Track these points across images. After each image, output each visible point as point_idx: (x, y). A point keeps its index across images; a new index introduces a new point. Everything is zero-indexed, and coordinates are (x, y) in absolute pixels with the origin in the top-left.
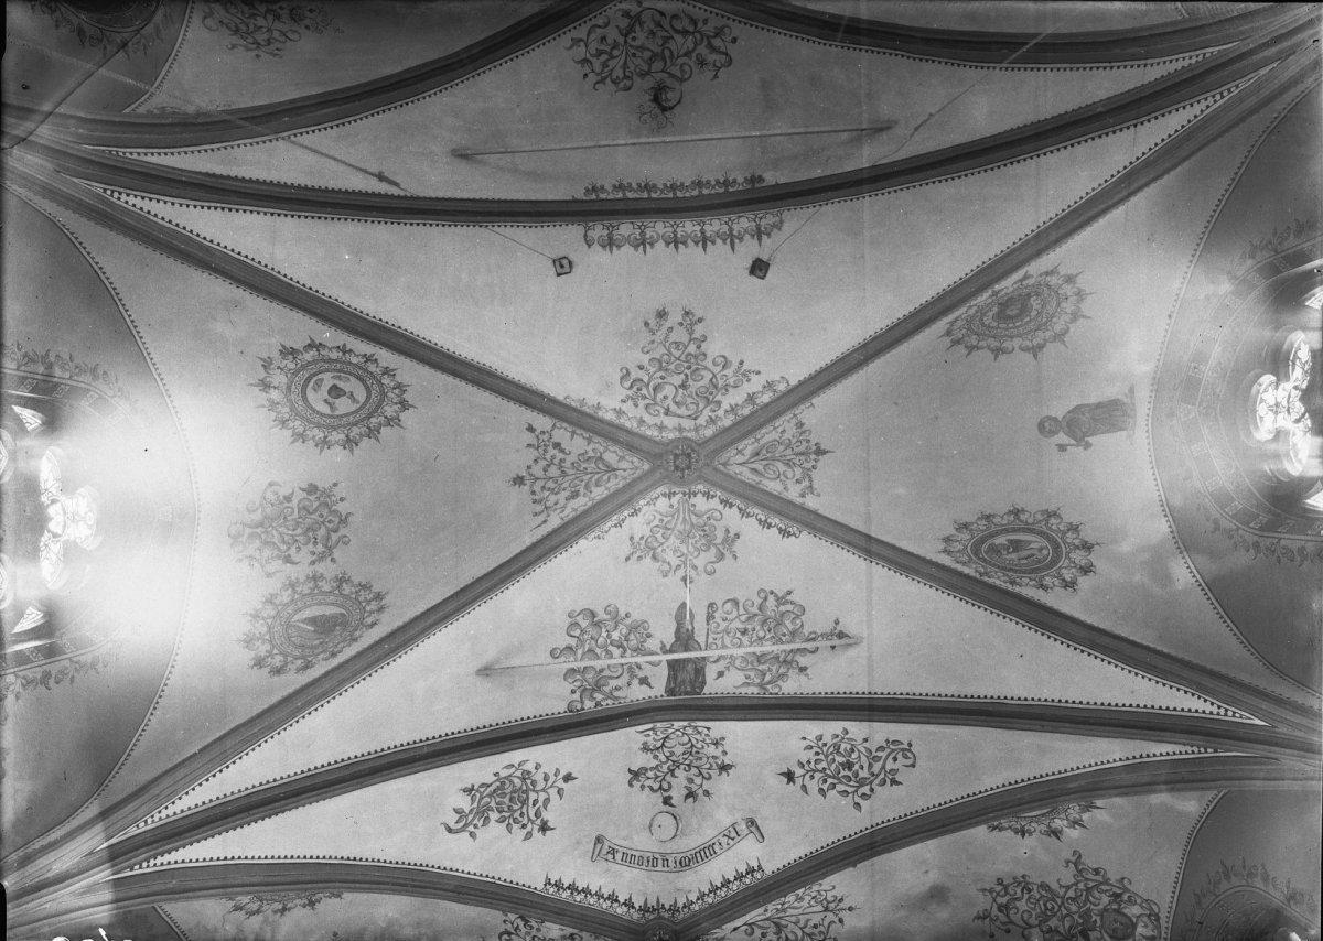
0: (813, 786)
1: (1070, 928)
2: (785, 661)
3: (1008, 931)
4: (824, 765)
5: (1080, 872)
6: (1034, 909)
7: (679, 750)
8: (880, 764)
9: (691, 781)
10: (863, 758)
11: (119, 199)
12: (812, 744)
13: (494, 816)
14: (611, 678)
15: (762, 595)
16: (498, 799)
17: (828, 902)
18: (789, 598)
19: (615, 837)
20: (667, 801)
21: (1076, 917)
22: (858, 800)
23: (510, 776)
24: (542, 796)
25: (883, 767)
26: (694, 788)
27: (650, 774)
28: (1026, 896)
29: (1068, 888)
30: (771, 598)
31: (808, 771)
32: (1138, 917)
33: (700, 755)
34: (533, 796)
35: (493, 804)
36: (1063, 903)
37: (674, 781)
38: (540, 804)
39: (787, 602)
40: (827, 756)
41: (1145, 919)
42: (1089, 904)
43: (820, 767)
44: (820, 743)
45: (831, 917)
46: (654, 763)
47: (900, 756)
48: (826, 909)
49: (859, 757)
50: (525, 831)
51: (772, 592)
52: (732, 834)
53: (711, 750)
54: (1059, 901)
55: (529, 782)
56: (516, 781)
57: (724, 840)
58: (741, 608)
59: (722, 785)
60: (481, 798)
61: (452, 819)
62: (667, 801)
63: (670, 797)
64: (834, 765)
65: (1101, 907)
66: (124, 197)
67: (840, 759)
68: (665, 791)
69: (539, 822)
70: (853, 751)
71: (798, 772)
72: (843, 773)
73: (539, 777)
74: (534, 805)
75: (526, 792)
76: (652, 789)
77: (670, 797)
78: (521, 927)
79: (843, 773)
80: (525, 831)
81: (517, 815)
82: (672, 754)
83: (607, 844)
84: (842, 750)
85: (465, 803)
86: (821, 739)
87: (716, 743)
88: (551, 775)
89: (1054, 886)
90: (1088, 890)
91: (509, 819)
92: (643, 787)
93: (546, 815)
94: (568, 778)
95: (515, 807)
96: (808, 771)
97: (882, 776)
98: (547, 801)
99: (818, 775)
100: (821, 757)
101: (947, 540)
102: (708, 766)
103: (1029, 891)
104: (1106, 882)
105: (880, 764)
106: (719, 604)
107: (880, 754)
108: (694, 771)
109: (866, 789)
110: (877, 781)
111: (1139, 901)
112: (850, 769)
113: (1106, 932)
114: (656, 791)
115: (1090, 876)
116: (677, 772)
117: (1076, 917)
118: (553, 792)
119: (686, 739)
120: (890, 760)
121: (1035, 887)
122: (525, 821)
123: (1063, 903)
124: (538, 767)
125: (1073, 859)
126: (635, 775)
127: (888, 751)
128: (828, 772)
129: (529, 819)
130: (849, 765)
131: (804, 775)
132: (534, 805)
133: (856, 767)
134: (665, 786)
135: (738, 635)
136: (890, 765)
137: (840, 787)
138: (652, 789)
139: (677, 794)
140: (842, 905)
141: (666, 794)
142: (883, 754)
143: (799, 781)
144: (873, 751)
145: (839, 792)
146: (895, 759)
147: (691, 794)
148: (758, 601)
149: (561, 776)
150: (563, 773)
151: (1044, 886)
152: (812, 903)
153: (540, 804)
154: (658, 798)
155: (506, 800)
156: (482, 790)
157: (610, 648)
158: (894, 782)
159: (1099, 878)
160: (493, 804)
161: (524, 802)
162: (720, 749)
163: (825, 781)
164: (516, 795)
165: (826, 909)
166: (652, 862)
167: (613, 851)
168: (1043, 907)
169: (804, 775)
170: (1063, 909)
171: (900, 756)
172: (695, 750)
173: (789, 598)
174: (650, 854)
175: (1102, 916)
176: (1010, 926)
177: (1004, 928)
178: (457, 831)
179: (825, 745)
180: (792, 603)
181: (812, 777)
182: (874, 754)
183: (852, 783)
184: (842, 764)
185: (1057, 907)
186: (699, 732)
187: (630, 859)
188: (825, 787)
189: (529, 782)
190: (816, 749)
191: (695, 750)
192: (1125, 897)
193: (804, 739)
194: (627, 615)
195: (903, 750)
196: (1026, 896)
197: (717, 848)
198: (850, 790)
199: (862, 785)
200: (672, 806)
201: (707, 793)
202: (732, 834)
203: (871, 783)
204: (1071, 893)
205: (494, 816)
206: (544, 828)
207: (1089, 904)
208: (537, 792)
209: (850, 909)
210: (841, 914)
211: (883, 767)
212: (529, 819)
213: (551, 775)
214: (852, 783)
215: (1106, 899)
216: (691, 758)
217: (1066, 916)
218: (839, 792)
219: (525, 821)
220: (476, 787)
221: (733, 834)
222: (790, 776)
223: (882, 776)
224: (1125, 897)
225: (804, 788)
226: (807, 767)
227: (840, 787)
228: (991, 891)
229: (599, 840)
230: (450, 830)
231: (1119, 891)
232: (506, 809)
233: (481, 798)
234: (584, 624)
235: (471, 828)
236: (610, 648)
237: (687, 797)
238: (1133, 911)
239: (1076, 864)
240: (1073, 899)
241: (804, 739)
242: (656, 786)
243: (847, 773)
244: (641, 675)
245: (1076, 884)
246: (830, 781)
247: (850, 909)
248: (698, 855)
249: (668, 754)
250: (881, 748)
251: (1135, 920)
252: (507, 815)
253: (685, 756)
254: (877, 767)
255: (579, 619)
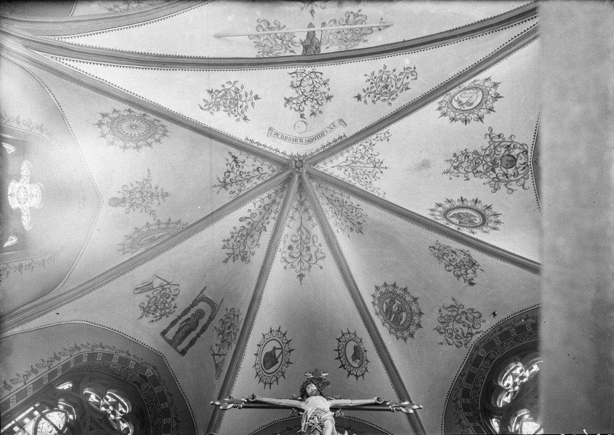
0: (369, 100)
1: (487, 169)
2: (357, 40)
3: (458, 176)
4: (375, 89)
5: (491, 139)
6: (470, 165)
7: (308, 89)
8: (400, 82)
9: (313, 107)
10: (393, 81)
11: (60, 61)
12: (370, 78)
13: (222, 108)
14: (277, 50)
15: (347, 15)
16: (224, 101)
17: (376, 163)
18: (360, 13)
19: (277, 128)
20: (302, 116)
21: (489, 163)
22: (390, 101)
23: (229, 89)
24: (245, 104)
25: (402, 83)
26: (315, 110)
27: (294, 101)
28: (466, 160)
29: (486, 150)
30: (352, 15)
31: (367, 94)
32: (518, 155)
33: (318, 92)
34: (240, 103)
35: (221, 103)
36: (483, 159)
37: (305, 107)
38: (244, 108)
39: (358, 16)
40: (376, 84)
41: (521, 155)
42: (495, 155)
43: (373, 90)
44: (373, 77)
45: (377, 170)
46: (296, 95)
47: (410, 76)
48: (375, 167)
49: (391, 81)
50: (237, 118)
51: (352, 12)
52: (332, 127)
53: (323, 89)
54: (482, 158)
55: (238, 95)
56: (232, 93)
57: (328, 130)
58: (337, 23)
59: (328, 107)
60: (216, 98)
61: (203, 104)
62: (302, 116)
63: (303, 115)
64: (379, 89)
65: (500, 156)
66: (62, 60)
67: (382, 84)
68: (301, 111)
69: (243, 115)
70: (388, 78)
71: (363, 94)
72: (383, 91)
73: (243, 93)
74: (241, 108)
75: (237, 100)
76: (295, 109)
77: (303, 115)
78: (235, 167)
79: (383, 91)
80: (237, 118)
81: (233, 110)
82: (305, 91)
83: (274, 131)
84: (383, 79)
85: (208, 97)
86: (374, 75)
87: (325, 84)
88: (249, 93)
89: (480, 151)
90: (495, 148)
91: (229, 111)
92: (291, 108)
93: (246, 114)
94: (256, 98)
95: (232, 107)
96: (367, 94)
97: (401, 88)
98: (247, 107)
99: (372, 95)
100: (374, 85)
101: (432, 210)
102: (321, 99)
103: (468, 157)
104: (504, 141)
105: (400, 82)
106: (327, 22)
107: (400, 77)
108: (315, 102)
109: (394, 96)
110: (399, 91)
111: (518, 146)
112: (387, 88)
113: (503, 167)
114: (297, 111)
115: (497, 140)
116: (307, 102)
117: (489, 163)
118: (249, 103)
119: (311, 82)
120: (405, 78)
121: (471, 154)
122: (237, 114)
123: (483, 159)
124: (242, 87)
125: (488, 133)
126: (288, 101)
127: (405, 74)
128: (376, 92)
129: (238, 113)
130: (386, 87)
131: (365, 96)
132: (241, 108)
133: (390, 86)
134: (301, 109)
135: (336, 34)
136: (406, 81)
137: (382, 98)
138: (295, 109)
139: (307, 113)
140: (382, 166)
141: (301, 113)
142: (402, 77)
143: (363, 99)
144: (398, 76)
145: (382, 100)
146: (408, 77)
147: (313, 114)
148: (345, 18)
149: (253, 95)
150: (254, 94)
151: (476, 152)
152: (369, 162)
153: (244, 108)
154: (298, 114)
155: (228, 102)
156: (217, 93)
157: (276, 39)
158: (407, 89)
159: (500, 140)
160: (221, 103)
161: (236, 105)
162: (327, 87)
163: (375, 97)
164: (232, 101)
165: (375, 167)
166: (296, 140)
167: (277, 134)
168: (474, 163)
169: (365, 96)
170: (483, 161)
171: (410, 76)
172: (315, 89)
173: (360, 13)
174: (293, 137)
175: (501, 160)
176: (459, 174)
177: (456, 175)
178: (205, 110)
179: (375, 77)
180: (361, 15)
181: (369, 96)
182: (398, 78)
183: (388, 95)
184: (383, 87)
185: (480, 162)
186: (317, 77)
187: (284, 138)
188: (375, 99)
189: (238, 95)
190: (371, 81)
191: (315, 89)
192: (512, 146)
193: (366, 75)
194: (284, 26)
195: (411, 72)
196: (466, 160)
197: (325, 133)
198: (386, 98)
199: (392, 94)
200: (304, 118)
201: (321, 112)
202: (332, 127)
203: (396, 92)
204: (487, 152)
205: (222, 108)
206: (245, 119)
207: (495, 155)
208: (242, 101)
209: (386, 168)
210: (382, 170)
211: (402, 83)
212: (238, 113)
213: (249, 93)
214: (388, 95)
215: (503, 150)
216: (313, 94)
217: (485, 164)
218: (382, 100)
219: (237, 114)
220: (214, 91)
221: (332, 126)
222: (359, 97)
223: (401, 88)
224: (512, 146)
225: (366, 102)
226: (367, 92)
227: (382, 98)
228: (451, 160)
229: (270, 129)
230: (201, 108)
231: (509, 144)
232: (228, 106)
233: (216, 98)
234: (264, 27)
235: (211, 110)
236: (276, 39)
237: (311, 115)
238: (515, 152)
239: (490, 135)
240: (488, 155)
241: (366, 75)
242: (297, 108)
243: (386, 90)
244: (291, 49)
245: (489, 147)
246: (377, 96)
247: (386, 168)
248: (316, 137)
249: (303, 91)
250: (401, 74)
251: (516, 157)
252: (228, 109)
253: (311, 93)
254: (399, 84)
255: (262, 24)
